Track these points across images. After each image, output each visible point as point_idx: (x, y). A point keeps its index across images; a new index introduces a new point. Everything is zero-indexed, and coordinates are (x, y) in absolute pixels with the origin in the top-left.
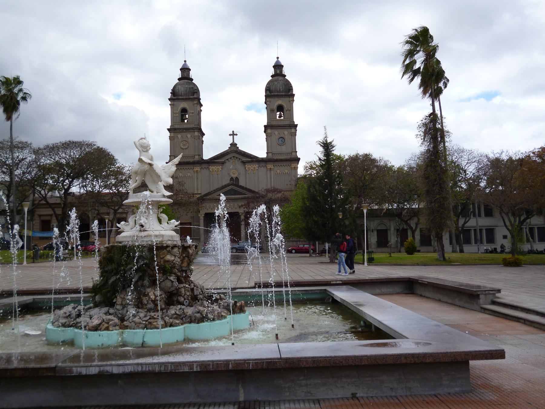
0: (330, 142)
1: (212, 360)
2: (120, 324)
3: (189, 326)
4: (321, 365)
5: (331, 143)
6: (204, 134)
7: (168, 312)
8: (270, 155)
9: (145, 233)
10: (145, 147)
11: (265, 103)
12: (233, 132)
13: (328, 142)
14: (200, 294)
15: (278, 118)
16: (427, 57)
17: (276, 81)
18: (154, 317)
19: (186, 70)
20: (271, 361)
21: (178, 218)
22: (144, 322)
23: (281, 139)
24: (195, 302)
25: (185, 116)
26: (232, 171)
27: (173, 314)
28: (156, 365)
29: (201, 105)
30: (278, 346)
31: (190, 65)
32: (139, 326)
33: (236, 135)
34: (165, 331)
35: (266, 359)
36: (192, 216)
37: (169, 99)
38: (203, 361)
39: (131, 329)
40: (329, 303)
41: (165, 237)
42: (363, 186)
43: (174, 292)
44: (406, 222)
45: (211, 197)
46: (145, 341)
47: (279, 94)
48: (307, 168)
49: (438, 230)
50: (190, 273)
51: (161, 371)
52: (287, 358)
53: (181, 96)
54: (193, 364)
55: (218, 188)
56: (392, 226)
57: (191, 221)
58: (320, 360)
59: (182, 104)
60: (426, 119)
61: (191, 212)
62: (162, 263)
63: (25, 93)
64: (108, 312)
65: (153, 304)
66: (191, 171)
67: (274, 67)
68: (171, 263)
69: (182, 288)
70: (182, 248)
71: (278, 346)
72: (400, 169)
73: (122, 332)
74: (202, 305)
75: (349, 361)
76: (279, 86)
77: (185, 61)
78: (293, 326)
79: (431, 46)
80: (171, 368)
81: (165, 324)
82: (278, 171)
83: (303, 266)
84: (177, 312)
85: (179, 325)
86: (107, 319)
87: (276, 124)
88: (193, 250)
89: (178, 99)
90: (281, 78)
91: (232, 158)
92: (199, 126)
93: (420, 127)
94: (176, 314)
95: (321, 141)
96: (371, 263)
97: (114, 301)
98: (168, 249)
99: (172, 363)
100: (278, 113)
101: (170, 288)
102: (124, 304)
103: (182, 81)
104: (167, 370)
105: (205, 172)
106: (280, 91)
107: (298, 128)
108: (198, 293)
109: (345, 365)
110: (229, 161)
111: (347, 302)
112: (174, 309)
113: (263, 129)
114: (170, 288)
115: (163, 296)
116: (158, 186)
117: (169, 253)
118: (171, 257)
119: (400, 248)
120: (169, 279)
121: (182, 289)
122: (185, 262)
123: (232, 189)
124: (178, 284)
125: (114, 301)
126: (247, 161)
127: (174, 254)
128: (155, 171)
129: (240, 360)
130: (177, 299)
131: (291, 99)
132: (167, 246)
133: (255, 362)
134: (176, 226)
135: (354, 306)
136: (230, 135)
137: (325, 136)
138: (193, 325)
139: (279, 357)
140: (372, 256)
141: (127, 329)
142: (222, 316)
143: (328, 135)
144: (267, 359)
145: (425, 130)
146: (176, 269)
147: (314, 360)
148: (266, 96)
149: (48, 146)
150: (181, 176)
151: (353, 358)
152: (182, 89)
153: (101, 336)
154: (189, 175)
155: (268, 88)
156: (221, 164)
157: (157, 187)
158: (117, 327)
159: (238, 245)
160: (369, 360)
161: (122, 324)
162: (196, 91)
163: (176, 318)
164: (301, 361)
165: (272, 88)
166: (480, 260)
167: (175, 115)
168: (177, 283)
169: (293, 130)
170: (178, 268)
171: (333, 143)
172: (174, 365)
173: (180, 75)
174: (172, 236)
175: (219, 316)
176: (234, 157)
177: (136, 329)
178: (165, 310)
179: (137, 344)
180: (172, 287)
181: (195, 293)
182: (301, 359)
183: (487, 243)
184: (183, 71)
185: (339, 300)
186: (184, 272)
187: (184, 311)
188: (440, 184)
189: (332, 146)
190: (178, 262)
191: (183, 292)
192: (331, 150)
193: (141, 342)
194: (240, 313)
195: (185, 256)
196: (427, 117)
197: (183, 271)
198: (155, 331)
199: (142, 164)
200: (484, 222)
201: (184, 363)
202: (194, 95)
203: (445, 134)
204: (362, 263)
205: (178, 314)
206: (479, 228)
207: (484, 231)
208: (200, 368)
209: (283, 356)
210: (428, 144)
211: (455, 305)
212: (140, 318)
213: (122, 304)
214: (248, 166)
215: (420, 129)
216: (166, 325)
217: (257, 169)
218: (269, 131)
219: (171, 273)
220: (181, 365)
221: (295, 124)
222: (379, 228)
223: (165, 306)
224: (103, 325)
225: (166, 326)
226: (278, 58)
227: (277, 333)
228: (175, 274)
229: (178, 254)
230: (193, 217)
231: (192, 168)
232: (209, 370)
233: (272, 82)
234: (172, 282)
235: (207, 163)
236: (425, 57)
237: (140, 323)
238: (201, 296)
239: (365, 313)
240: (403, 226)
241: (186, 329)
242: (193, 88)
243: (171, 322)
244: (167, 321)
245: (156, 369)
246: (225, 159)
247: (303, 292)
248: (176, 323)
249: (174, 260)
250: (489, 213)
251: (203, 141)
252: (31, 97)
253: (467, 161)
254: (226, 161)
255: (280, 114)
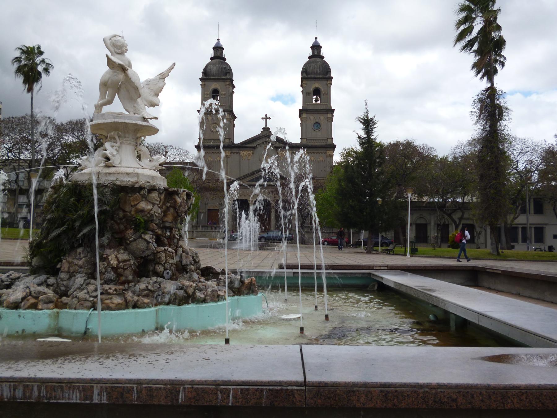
0: (371, 119)
1: (138, 380)
2: (57, 301)
3: (164, 309)
4: (403, 405)
5: (373, 120)
6: (235, 118)
7: (137, 285)
8: (304, 140)
9: (112, 170)
10: (120, 46)
11: (301, 86)
12: (266, 115)
13: (369, 118)
14: (191, 264)
15: (314, 102)
16: (486, 24)
17: (314, 62)
18: (109, 291)
19: (219, 49)
20: (282, 389)
22: (92, 299)
23: (316, 125)
24: (181, 275)
25: (216, 97)
27: (143, 289)
28: (4, 384)
29: (234, 87)
30: (301, 350)
31: (223, 44)
32: (82, 304)
33: (270, 118)
34: (123, 313)
35: (269, 382)
37: (201, 79)
38: (117, 381)
39: (70, 308)
40: (374, 291)
41: (141, 177)
42: (404, 174)
43: (149, 257)
44: (449, 215)
46: (88, 329)
47: (316, 76)
48: (344, 155)
49: (493, 220)
50: (177, 233)
51: (16, 398)
52: (320, 383)
53: (213, 76)
54: (93, 387)
55: (248, 174)
56: (432, 221)
57: (219, 208)
58: (402, 392)
59: (213, 85)
60: (482, 94)
62: (133, 213)
63: (47, 64)
64: (46, 281)
65: (114, 272)
67: (311, 47)
68: (146, 213)
69: (162, 252)
70: (164, 193)
71: (301, 350)
72: (444, 159)
73: (58, 313)
74: (191, 279)
75: (473, 397)
76: (317, 67)
77: (218, 40)
78: (327, 316)
79: (491, 11)
80: (40, 393)
81: (124, 304)
83: (337, 254)
84: (150, 287)
85: (149, 307)
86: (37, 292)
87: (312, 108)
88: (183, 199)
89: (210, 79)
90: (318, 60)
92: (231, 108)
93: (475, 103)
94: (147, 289)
95: (362, 118)
96: (414, 254)
97: (58, 266)
98: (142, 192)
99: (43, 382)
100: (315, 97)
101: (144, 251)
102: (71, 271)
103: (214, 61)
104: (30, 397)
106: (317, 73)
107: (334, 114)
108: (188, 263)
109: (462, 407)
110: (261, 146)
111: (406, 286)
112: (146, 282)
113: (298, 113)
114: (144, 251)
115: (132, 262)
116: (136, 105)
117: (144, 199)
118: (148, 205)
119: (440, 244)
120: (142, 238)
121: (162, 253)
122: (169, 214)
124: (157, 246)
125: (58, 266)
127: (152, 201)
128: (130, 79)
129: (206, 383)
130: (154, 268)
131: (329, 82)
132: (141, 188)
133: (242, 389)
134: (160, 165)
135: (421, 291)
136: (263, 118)
137: (366, 111)
138: (172, 307)
139: (300, 379)
140: (416, 248)
141: (66, 308)
142: (219, 296)
143: (369, 111)
144: (270, 384)
145: (481, 107)
146: (155, 223)
147: (388, 392)
148: (302, 78)
149: (70, 122)
151: (484, 392)
152: (214, 69)
153: (22, 316)
155: (304, 70)
157: (134, 107)
158: (51, 305)
159: (268, 234)
160: (523, 397)
161: (59, 300)
162: (228, 71)
163: (147, 296)
164: (353, 391)
165: (310, 70)
166: (540, 256)
167: (206, 96)
168: (155, 245)
169: (330, 115)
170: (157, 222)
171: (374, 120)
172: (46, 387)
173: (213, 54)
174: (153, 177)
175: (214, 295)
177: (78, 309)
178: (133, 283)
179: (77, 333)
180: (147, 249)
181: (184, 262)
182: (355, 389)
183: (535, 243)
184: (216, 49)
185: (392, 285)
186: (168, 230)
187: (160, 285)
188: (497, 168)
189: (373, 122)
190: (159, 214)
191: (164, 258)
192: (373, 127)
193: (83, 330)
194: (248, 294)
195: (170, 206)
196: (484, 91)
197: (166, 228)
198: (106, 314)
199: (115, 72)
200: (534, 219)
201: (70, 383)
202: (226, 76)
203: (504, 110)
204: (404, 254)
205: (150, 290)
206: (529, 226)
207: (533, 229)
208: (108, 399)
209: (311, 378)
210: (485, 121)
211: (544, 301)
212: (88, 292)
213: (68, 272)
215: (476, 105)
216: (126, 305)
218: (304, 115)
219: (147, 229)
220: (62, 388)
221: (332, 108)
222: (418, 222)
223: (134, 277)
224: (28, 300)
225: (127, 307)
226: (316, 38)
227: (302, 326)
228: (153, 231)
229: (158, 201)
232: (128, 403)
233: (309, 63)
234: (148, 243)
236: (483, 24)
237: (86, 300)
238: (192, 267)
239: (443, 300)
240: (445, 221)
241: (160, 311)
242: (225, 68)
243: (136, 300)
244: (129, 298)
245: (5, 394)
247: (340, 275)
248: (144, 303)
249: (151, 210)
250: (539, 210)
251: (234, 125)
252: (53, 68)
253: (519, 151)
254: (257, 145)
255: (317, 98)
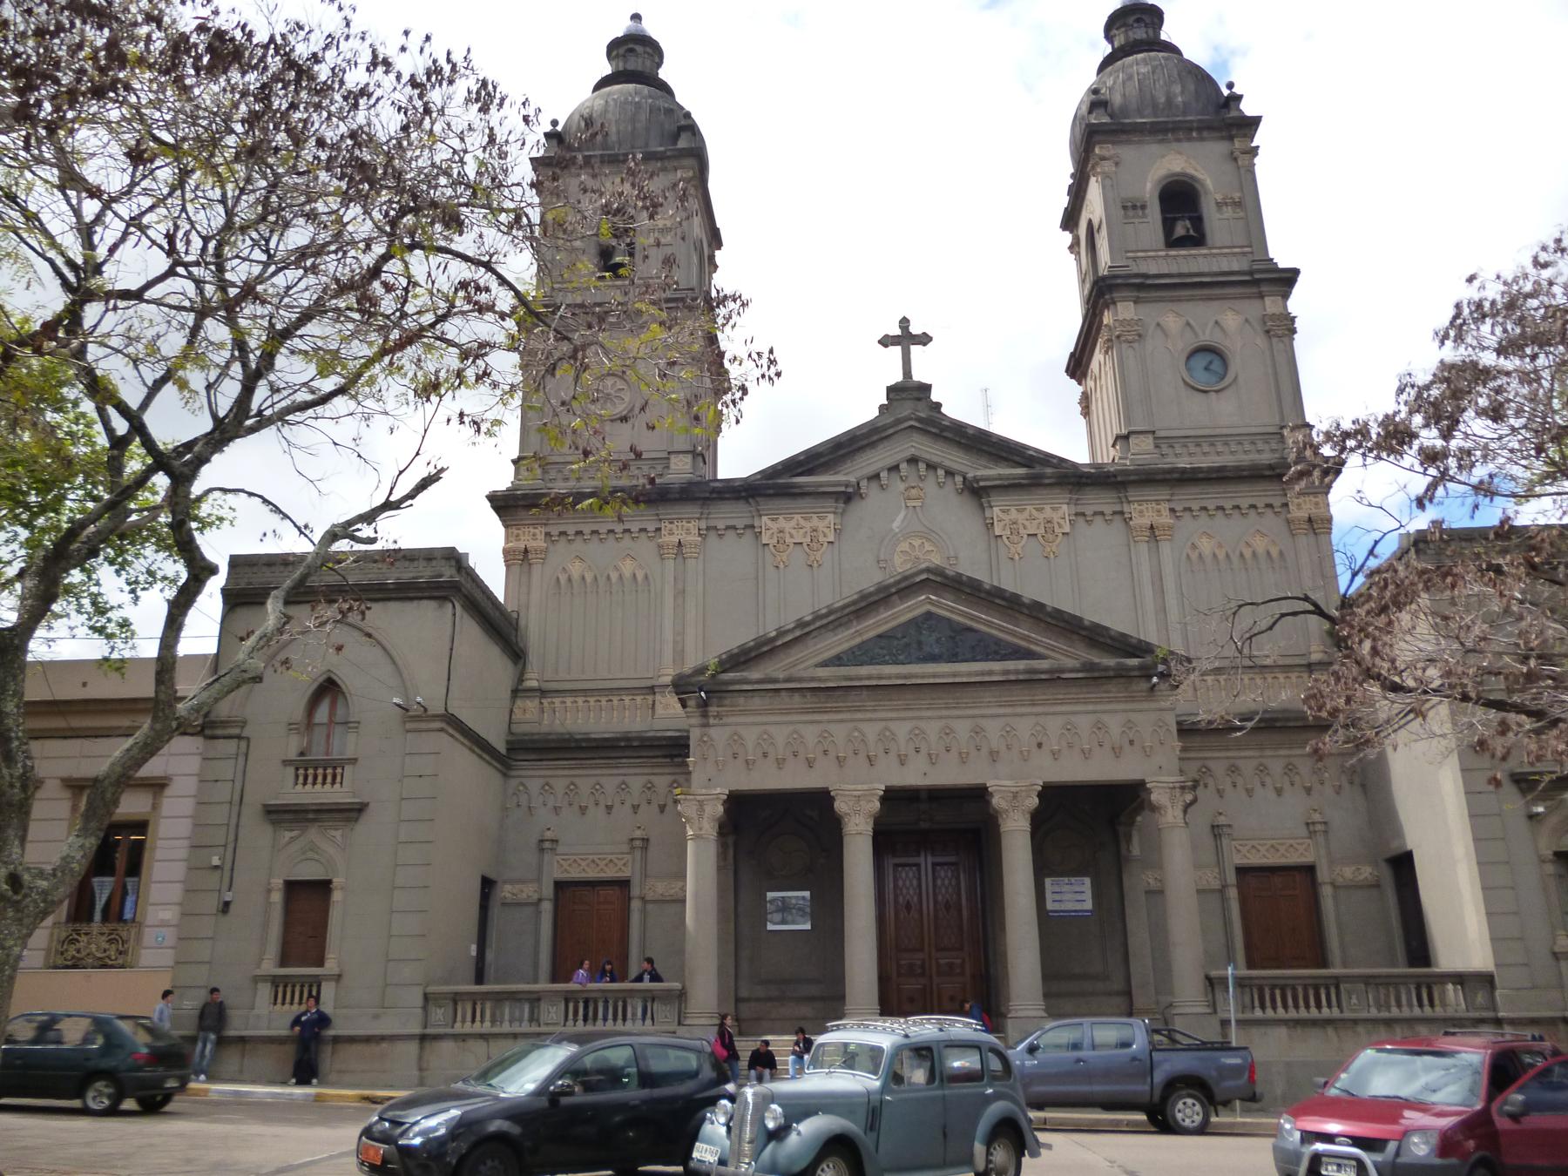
12: (904, 323)
19: (639, 49)
21: (542, 850)
23: (1201, 361)
26: (904, 546)
33: (924, 339)
36: (638, 834)
45: (773, 668)
57: (625, 873)
61: (635, 808)
66: (645, 547)
82: (1206, 546)
91: (903, 466)
105: (732, 554)
123: (929, 615)
126: (1000, 477)
136: (886, 341)
150: (576, 576)
154: (627, 573)
156: (830, 504)
176: (913, 461)
214: (1002, 511)
217: (1067, 529)
230: (646, 840)
231: (651, 527)
235: (746, 499)
246: (859, 474)
254: (864, 483)
